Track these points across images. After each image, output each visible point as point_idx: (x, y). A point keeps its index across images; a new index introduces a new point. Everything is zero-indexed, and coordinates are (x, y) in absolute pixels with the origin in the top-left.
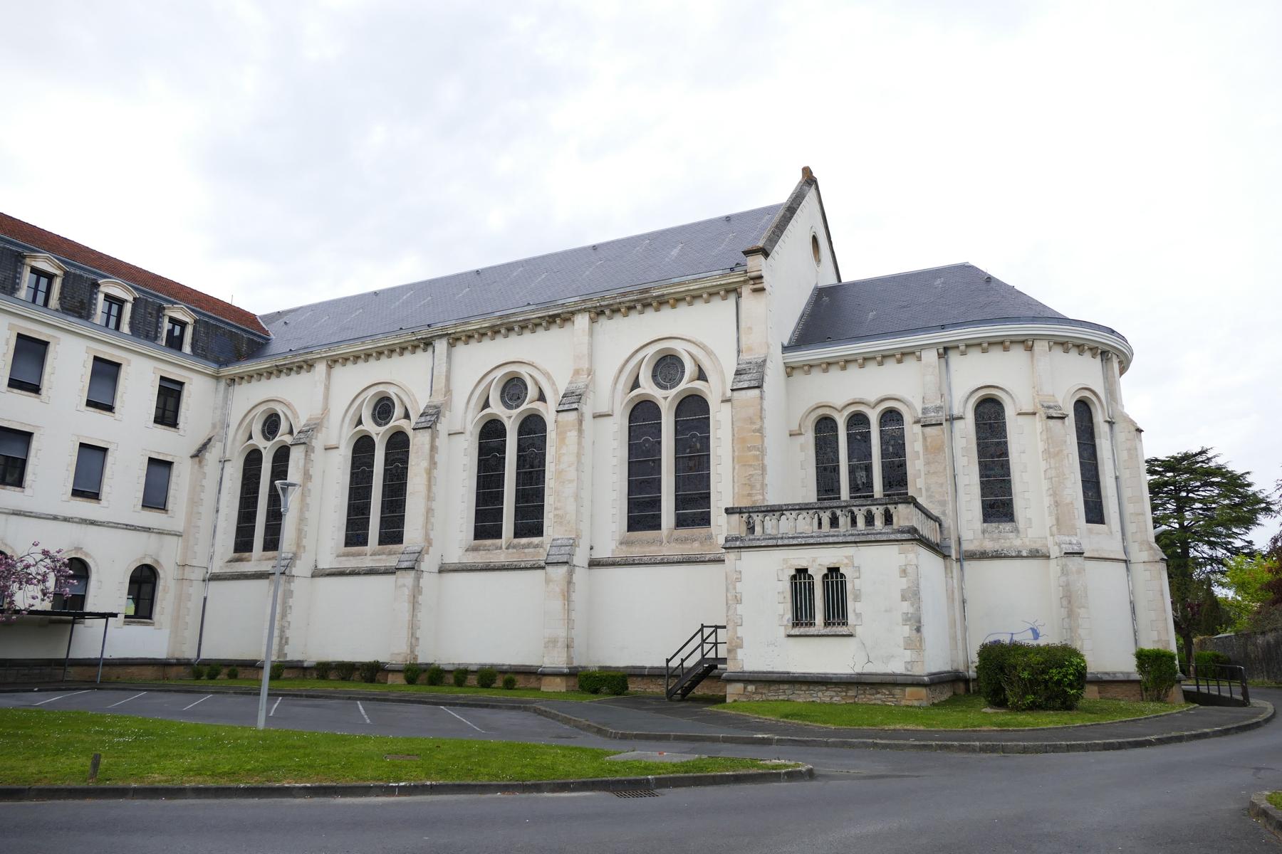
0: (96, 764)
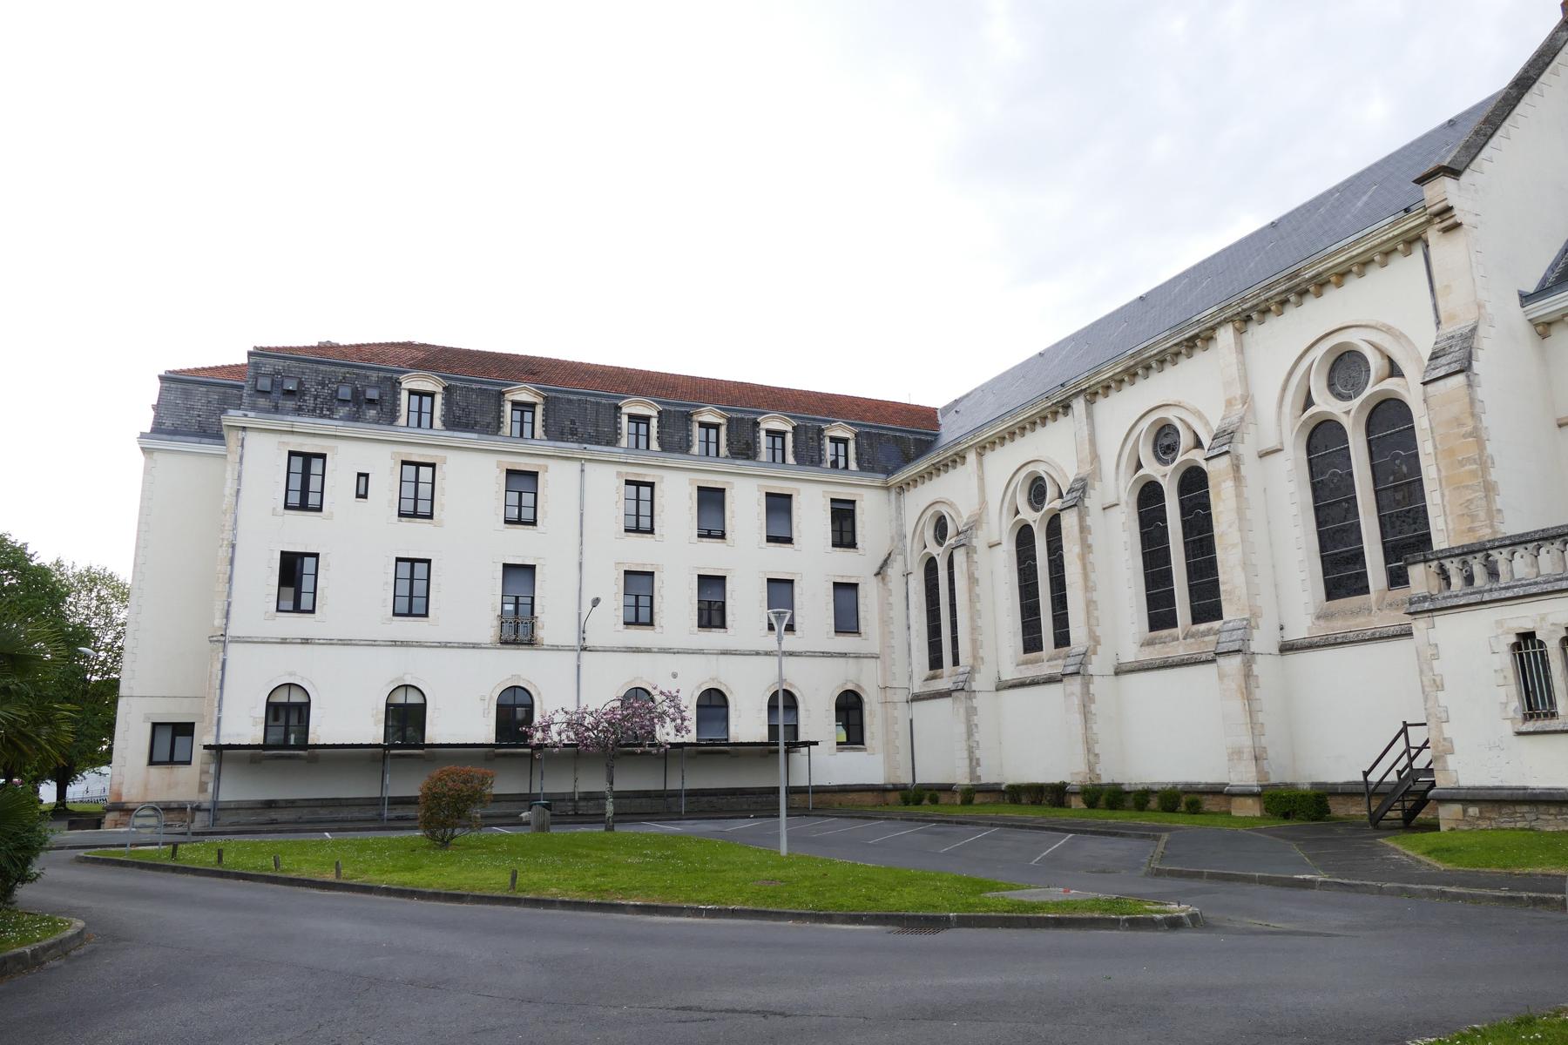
0: (514, 878)
